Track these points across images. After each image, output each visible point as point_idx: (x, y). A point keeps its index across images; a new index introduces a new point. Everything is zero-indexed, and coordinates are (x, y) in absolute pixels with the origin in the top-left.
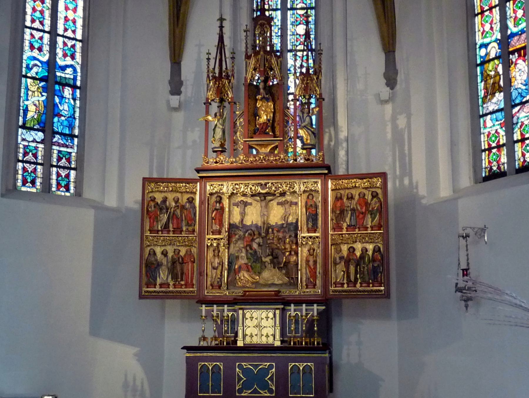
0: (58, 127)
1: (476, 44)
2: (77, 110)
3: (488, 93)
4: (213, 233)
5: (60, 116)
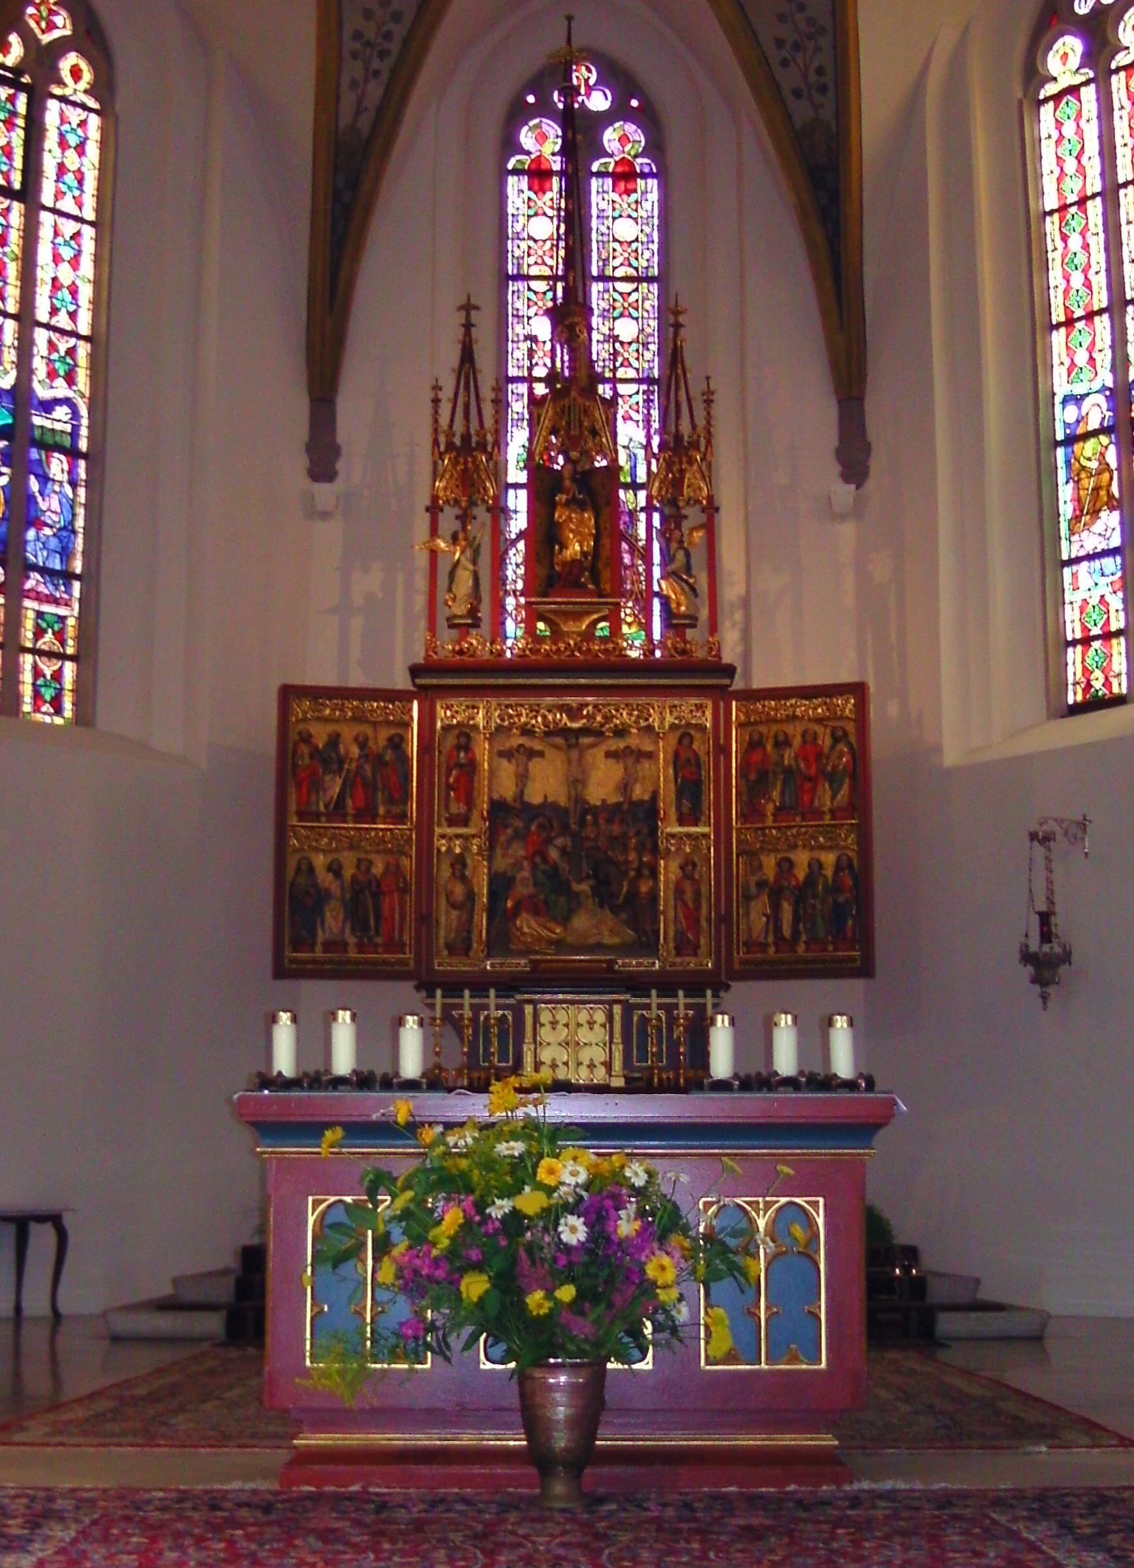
0: (36, 553)
1: (1054, 394)
2: (81, 511)
3: (1082, 511)
4: (452, 822)
5: (39, 524)
